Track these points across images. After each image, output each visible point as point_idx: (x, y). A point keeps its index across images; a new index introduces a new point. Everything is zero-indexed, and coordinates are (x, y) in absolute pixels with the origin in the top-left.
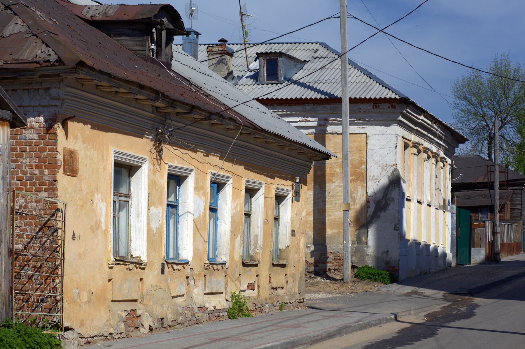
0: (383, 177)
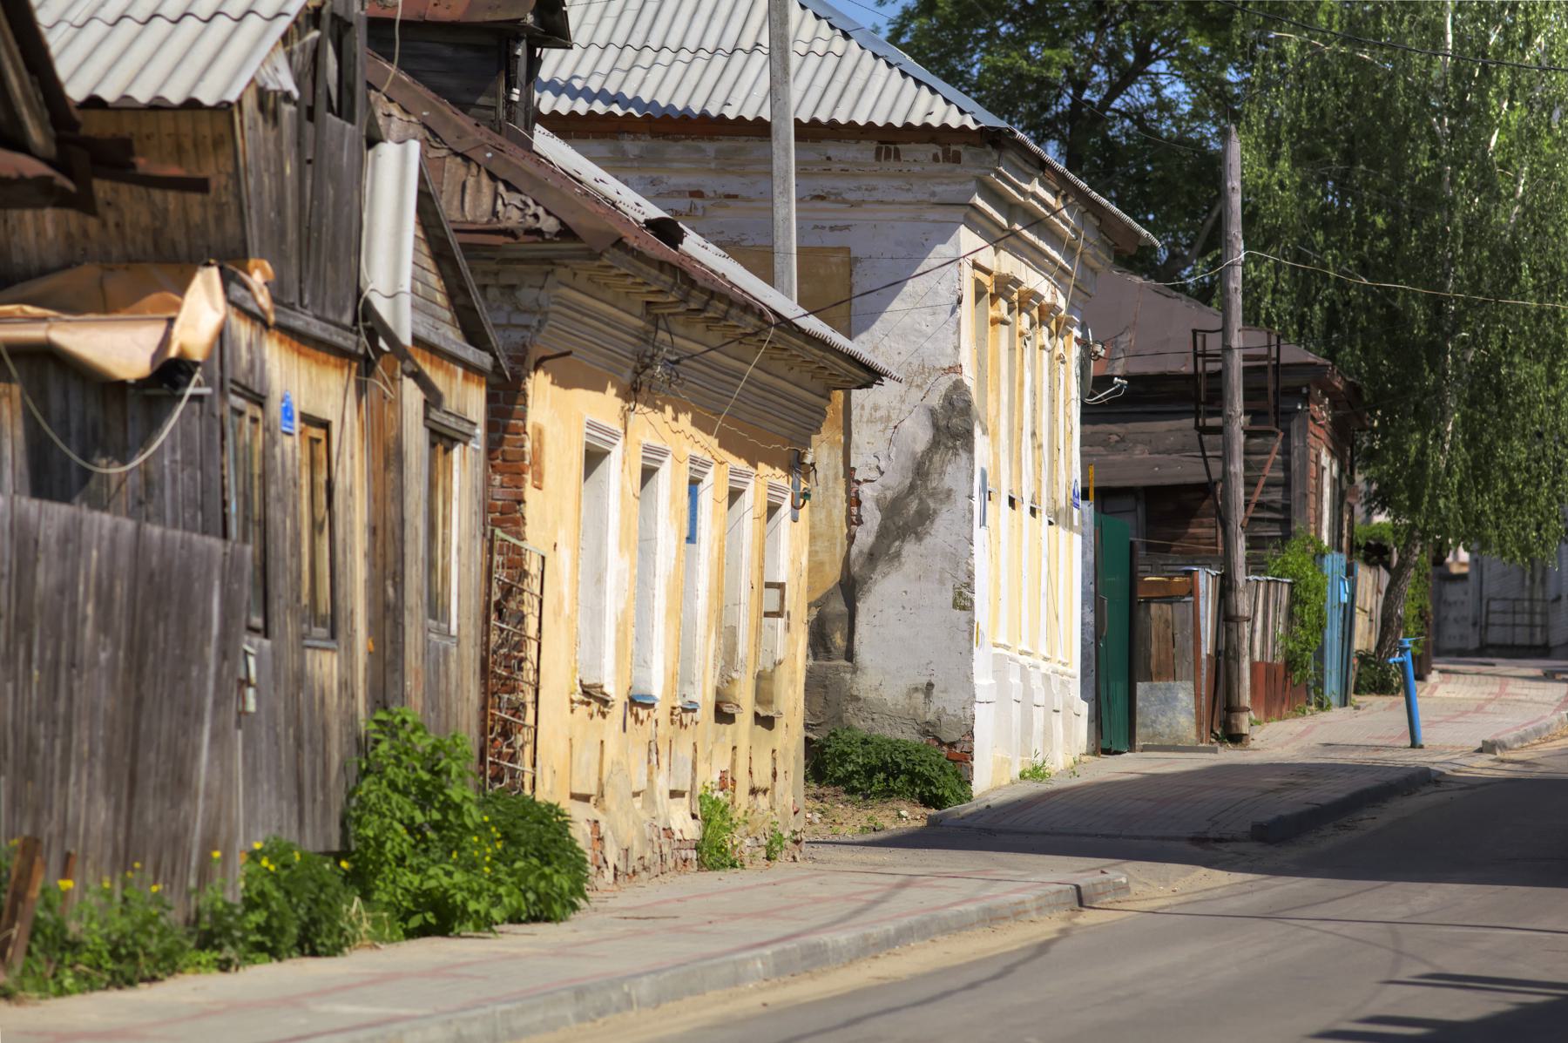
0: (911, 413)
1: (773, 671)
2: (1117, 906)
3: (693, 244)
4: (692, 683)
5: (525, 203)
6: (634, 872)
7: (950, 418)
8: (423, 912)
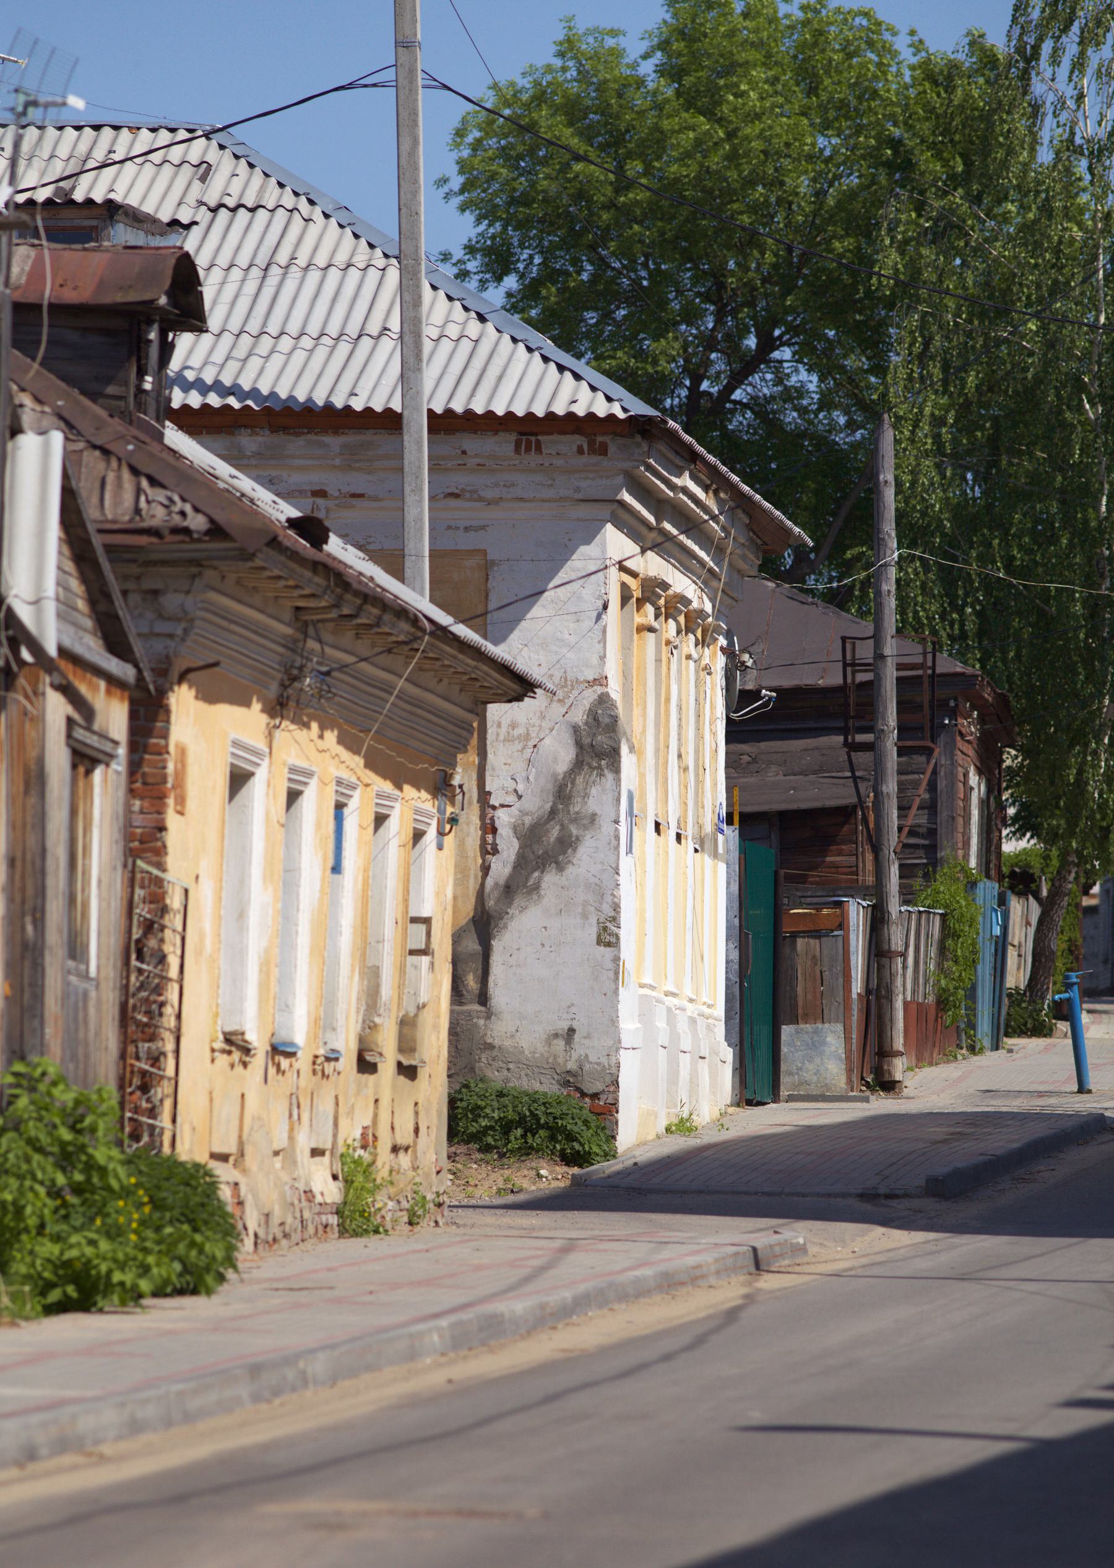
0: (552, 730)
1: (416, 1015)
2: (797, 1269)
3: (335, 546)
4: (334, 1029)
5: (171, 500)
6: (275, 1240)
7: (594, 735)
8: (63, 1285)
